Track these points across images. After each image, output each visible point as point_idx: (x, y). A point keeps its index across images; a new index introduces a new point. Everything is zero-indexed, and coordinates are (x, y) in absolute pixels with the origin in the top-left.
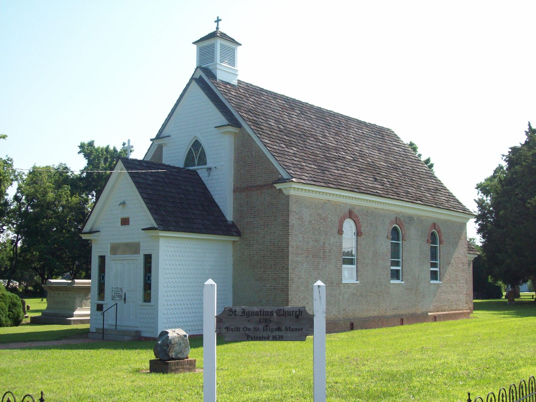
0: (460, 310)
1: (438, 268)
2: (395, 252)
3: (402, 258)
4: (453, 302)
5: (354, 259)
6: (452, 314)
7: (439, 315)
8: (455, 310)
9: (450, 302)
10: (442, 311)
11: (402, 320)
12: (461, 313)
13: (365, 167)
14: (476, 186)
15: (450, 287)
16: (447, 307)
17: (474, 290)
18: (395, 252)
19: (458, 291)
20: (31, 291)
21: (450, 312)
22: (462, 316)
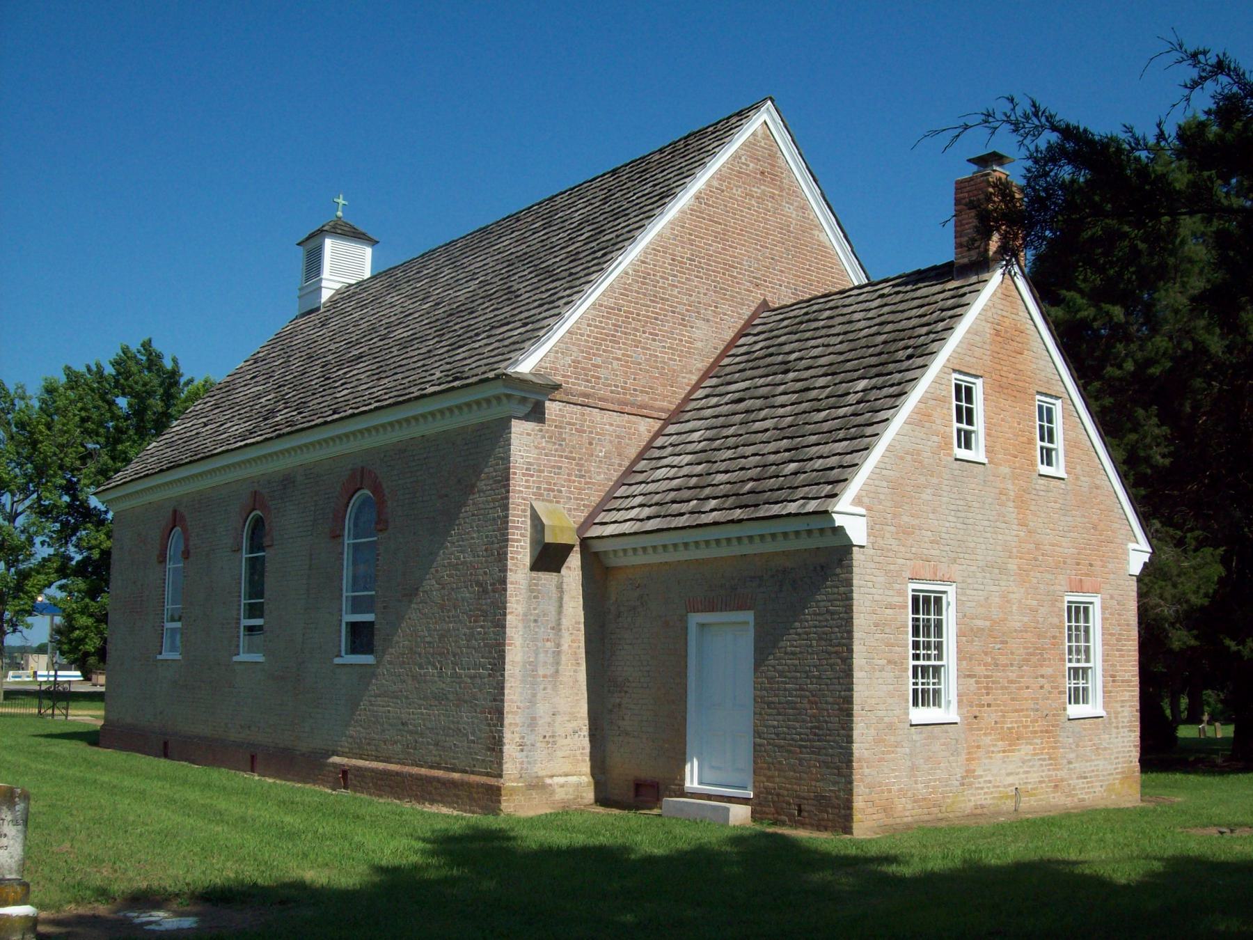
0: (454, 770)
1: (347, 623)
2: (256, 588)
3: (240, 605)
4: (422, 735)
5: (247, 597)
6: (411, 775)
7: (359, 769)
8: (431, 767)
9: (411, 732)
10: (377, 759)
11: (253, 757)
12: (454, 783)
13: (535, 280)
14: (1206, 109)
15: (414, 678)
16: (398, 747)
17: (1142, 761)
18: (256, 588)
19: (451, 697)
20: (1043, 196)
21: (406, 769)
22: (458, 796)
